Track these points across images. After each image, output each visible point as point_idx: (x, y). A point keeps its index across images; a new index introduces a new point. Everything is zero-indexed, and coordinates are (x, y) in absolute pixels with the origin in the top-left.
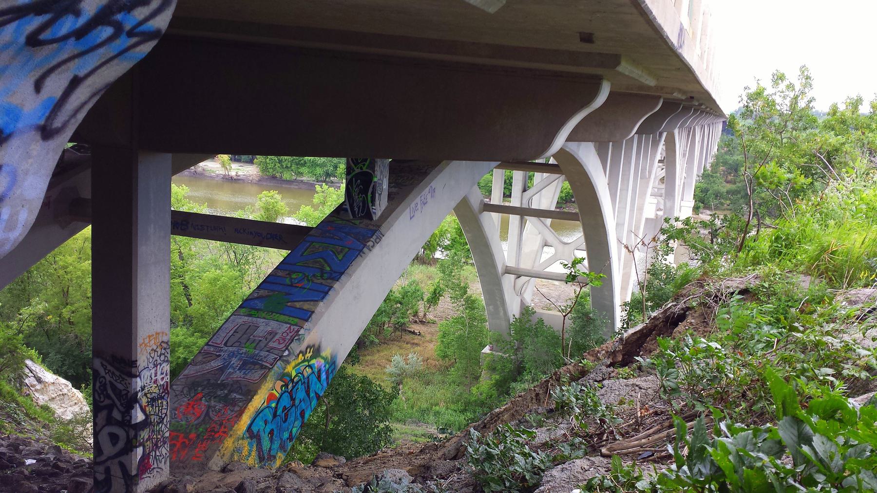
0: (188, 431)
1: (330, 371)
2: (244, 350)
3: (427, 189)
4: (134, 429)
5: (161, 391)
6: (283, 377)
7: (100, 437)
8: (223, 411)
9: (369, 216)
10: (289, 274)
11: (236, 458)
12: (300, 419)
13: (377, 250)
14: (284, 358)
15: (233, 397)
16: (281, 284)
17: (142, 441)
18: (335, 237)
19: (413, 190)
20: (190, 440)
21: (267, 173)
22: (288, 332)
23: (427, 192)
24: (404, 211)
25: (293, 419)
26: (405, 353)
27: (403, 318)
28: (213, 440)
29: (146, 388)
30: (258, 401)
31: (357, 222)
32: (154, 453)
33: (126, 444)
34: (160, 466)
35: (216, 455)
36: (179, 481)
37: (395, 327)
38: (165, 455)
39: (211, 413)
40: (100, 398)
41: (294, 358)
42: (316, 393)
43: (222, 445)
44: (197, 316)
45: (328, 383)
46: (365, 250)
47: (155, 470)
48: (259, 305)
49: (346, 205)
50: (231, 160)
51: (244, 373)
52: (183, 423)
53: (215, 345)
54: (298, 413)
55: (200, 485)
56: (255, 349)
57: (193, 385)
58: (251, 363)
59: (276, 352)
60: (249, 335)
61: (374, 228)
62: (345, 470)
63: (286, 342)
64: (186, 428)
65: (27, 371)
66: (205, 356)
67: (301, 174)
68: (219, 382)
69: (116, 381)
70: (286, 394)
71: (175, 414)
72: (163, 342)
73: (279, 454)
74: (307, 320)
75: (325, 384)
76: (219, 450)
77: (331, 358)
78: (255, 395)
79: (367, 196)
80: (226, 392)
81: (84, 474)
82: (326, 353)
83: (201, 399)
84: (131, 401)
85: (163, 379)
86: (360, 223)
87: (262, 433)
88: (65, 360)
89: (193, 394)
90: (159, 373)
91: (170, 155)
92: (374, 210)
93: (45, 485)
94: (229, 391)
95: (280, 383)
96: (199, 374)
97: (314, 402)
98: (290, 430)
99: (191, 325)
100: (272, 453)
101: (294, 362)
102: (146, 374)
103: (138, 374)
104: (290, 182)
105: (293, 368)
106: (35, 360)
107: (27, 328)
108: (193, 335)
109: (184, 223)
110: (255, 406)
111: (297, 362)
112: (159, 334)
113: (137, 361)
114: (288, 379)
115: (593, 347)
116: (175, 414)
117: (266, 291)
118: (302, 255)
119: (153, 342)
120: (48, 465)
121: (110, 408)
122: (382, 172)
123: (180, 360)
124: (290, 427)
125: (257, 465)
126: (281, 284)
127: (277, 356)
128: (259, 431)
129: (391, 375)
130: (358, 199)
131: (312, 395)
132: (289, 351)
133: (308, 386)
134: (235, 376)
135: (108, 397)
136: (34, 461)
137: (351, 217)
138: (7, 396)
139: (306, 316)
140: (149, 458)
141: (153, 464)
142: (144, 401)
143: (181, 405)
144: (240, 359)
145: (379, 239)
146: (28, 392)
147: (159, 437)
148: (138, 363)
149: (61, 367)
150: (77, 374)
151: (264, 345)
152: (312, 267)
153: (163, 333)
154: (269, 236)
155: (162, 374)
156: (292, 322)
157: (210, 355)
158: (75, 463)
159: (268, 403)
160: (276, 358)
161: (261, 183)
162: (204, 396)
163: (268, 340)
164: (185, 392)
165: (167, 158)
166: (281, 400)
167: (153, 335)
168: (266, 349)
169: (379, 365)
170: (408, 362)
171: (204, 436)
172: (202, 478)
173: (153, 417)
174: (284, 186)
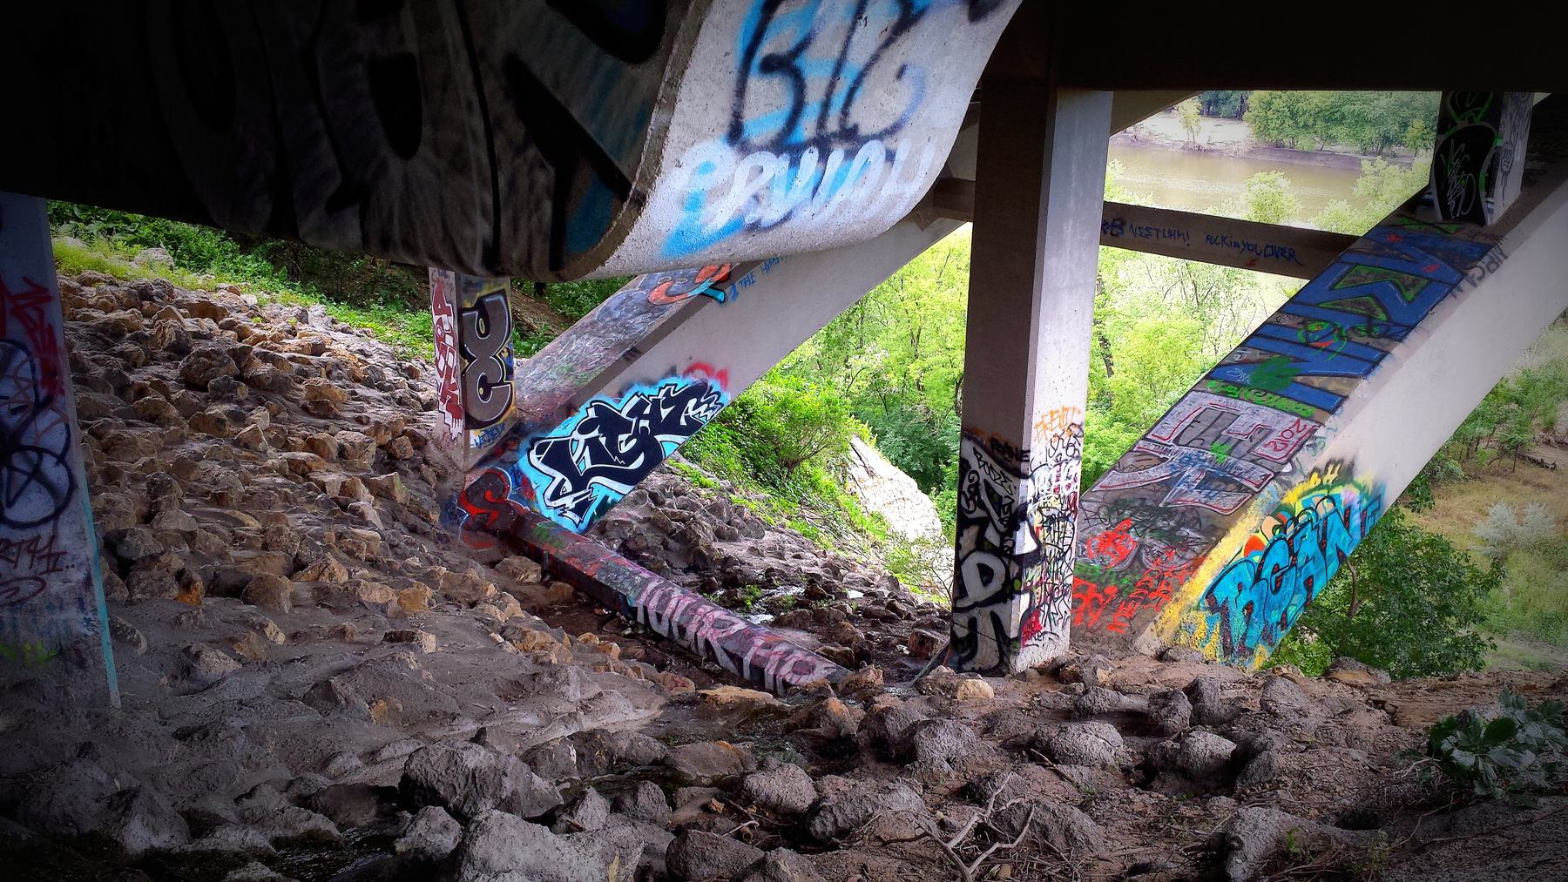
4: (1018, 564)
5: (1065, 506)
6: (1277, 510)
7: (964, 568)
8: (1165, 556)
9: (1477, 216)
11: (1183, 639)
12: (1305, 592)
15: (1185, 534)
17: (1029, 584)
18: (1404, 256)
20: (1106, 596)
21: (1267, 139)
22: (1293, 429)
25: (1290, 589)
27: (1520, 432)
28: (1145, 602)
29: (1041, 498)
30: (1229, 548)
31: (1452, 228)
32: (1047, 607)
33: (1004, 585)
35: (1148, 630)
36: (1086, 661)
37: (1502, 449)
39: (1144, 556)
40: (969, 506)
41: (1302, 478)
42: (1339, 551)
44: (1121, 393)
45: (1363, 534)
46: (1464, 284)
47: (1047, 636)
49: (1430, 193)
51: (1206, 496)
52: (1096, 565)
53: (1159, 441)
54: (1302, 580)
55: (1120, 674)
57: (1116, 505)
59: (1269, 464)
60: (1220, 429)
62: (1391, 696)
63: (1288, 449)
64: (1100, 576)
66: (1138, 458)
67: (1332, 139)
68: (1161, 505)
70: (1282, 543)
71: (1084, 550)
74: (1332, 412)
75: (1357, 536)
76: (1155, 622)
77: (1374, 487)
78: (1224, 535)
80: (1172, 523)
81: (933, 626)
82: (1365, 476)
83: (1128, 530)
84: (1017, 517)
87: (1231, 606)
88: (908, 446)
89: (1115, 521)
91: (1111, 94)
92: (1490, 206)
93: (874, 633)
94: (1177, 523)
95: (1272, 522)
96: (1127, 486)
97: (1333, 566)
99: (1108, 408)
100: (1248, 643)
101: (1301, 486)
102: (1042, 474)
103: (1030, 473)
104: (1307, 155)
105: (1299, 498)
106: (867, 440)
107: (857, 390)
108: (1112, 425)
110: (1222, 555)
113: (1029, 451)
114: (1288, 516)
116: (1084, 550)
117: (1258, 352)
118: (1331, 289)
119: (1056, 423)
120: (880, 603)
121: (983, 523)
122: (1514, 128)
123: (1090, 465)
124: (1285, 604)
125: (1218, 660)
128: (1226, 601)
130: (1458, 184)
131: (1330, 551)
132: (1293, 464)
133: (1324, 535)
134: (1189, 497)
135: (981, 505)
136: (861, 595)
137: (1440, 217)
138: (824, 491)
139: (1332, 403)
142: (1036, 520)
144: (1201, 470)
146: (854, 489)
147: (1056, 582)
148: (1032, 455)
149: (903, 457)
150: (925, 470)
151: (1247, 449)
152: (1351, 312)
153: (1074, 409)
154: (1269, 251)
156: (1303, 414)
157: (1147, 457)
158: (919, 607)
159: (1246, 553)
161: (1253, 156)
162: (1133, 526)
163: (1254, 442)
164: (1102, 515)
165: (1104, 101)
166: (1271, 552)
168: (1249, 457)
169: (1459, 518)
170: (1524, 520)
171: (1130, 594)
172: (1122, 664)
173: (1048, 548)
174: (1296, 162)
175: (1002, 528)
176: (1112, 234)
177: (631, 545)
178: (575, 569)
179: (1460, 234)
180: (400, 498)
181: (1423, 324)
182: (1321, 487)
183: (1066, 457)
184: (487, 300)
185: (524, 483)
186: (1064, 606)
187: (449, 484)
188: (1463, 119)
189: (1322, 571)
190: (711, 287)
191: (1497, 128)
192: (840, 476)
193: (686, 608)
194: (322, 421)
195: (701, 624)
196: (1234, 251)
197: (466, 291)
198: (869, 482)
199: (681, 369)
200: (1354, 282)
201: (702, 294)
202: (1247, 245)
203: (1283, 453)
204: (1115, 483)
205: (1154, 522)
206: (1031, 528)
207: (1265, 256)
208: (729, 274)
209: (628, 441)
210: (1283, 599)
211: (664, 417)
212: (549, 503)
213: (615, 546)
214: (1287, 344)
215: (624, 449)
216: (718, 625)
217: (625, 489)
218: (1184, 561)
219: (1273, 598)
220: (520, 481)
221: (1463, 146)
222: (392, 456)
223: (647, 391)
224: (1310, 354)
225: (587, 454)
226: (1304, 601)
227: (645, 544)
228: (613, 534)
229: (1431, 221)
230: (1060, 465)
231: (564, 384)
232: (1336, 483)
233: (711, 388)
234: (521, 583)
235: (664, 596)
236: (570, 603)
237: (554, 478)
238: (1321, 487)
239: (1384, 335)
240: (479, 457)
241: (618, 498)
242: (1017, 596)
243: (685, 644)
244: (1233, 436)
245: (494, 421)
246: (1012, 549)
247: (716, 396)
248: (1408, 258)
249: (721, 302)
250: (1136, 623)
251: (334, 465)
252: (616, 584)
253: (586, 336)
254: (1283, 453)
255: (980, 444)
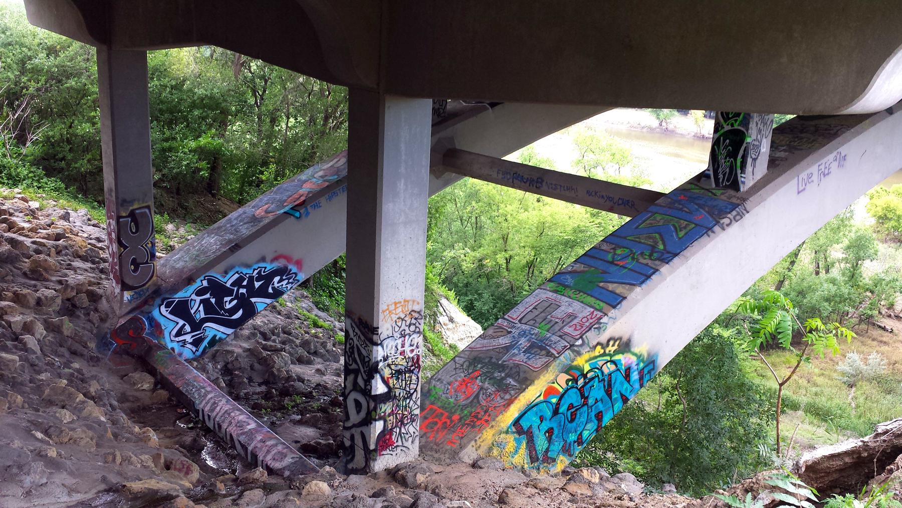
0: (453, 411)
1: (646, 371)
2: (536, 331)
3: (831, 157)
4: (373, 401)
5: (410, 364)
9: (735, 185)
10: (614, 249)
11: (495, 452)
12: (596, 422)
13: (735, 229)
14: (576, 348)
15: (508, 382)
16: (602, 260)
19: (808, 156)
20: (452, 421)
23: (831, 160)
24: (788, 182)
26: (867, 350)
28: (473, 427)
29: (390, 358)
30: (533, 393)
31: (719, 192)
32: (398, 430)
34: (406, 444)
35: (470, 446)
38: (413, 434)
39: (481, 395)
41: (588, 349)
42: (622, 395)
43: (481, 435)
46: (717, 228)
47: (399, 449)
48: (570, 280)
50: (705, 116)
51: (528, 357)
52: (452, 400)
54: (593, 414)
56: (548, 331)
58: (539, 347)
59: (569, 339)
60: (547, 314)
61: (738, 202)
63: (582, 329)
65: (441, 310)
68: (500, 362)
69: (361, 345)
70: (574, 390)
71: (448, 389)
72: (413, 311)
73: (561, 457)
74: (614, 307)
76: (476, 441)
77: (649, 355)
78: (530, 385)
79: (736, 160)
83: (476, 378)
84: (373, 370)
85: (412, 351)
86: (722, 194)
88: (497, 303)
90: (407, 344)
92: (743, 179)
98: (579, 433)
100: (550, 454)
101: (587, 354)
109: (540, 180)
110: (527, 398)
111: (592, 354)
112: (408, 301)
113: (378, 328)
114: (578, 373)
115: (731, 480)
116: (448, 389)
117: (583, 266)
118: (637, 228)
119: (400, 309)
121: (356, 372)
122: (760, 131)
126: (602, 260)
127: (567, 344)
128: (531, 427)
129: (843, 374)
131: (615, 395)
132: (583, 340)
135: (355, 361)
137: (714, 186)
139: (615, 301)
140: (391, 435)
141: (397, 441)
142: (387, 373)
143: (456, 381)
144: (529, 341)
145: (741, 216)
146: (440, 330)
147: (406, 413)
154: (620, 202)
155: (411, 345)
156: (598, 307)
160: (565, 346)
162: (480, 375)
166: (566, 396)
167: (401, 302)
169: (831, 360)
175: (365, 377)
176: (536, 187)
177: (230, 366)
178: (171, 383)
179: (724, 195)
180: (66, 332)
181: (685, 253)
182: (604, 354)
183: (409, 332)
184: (137, 211)
185: (157, 328)
186: (413, 429)
187: (107, 325)
188: (728, 125)
189: (609, 408)
190: (292, 209)
191: (747, 130)
192: (432, 322)
193: (225, 412)
194: (33, 282)
195: (230, 423)
196: (602, 201)
197: (122, 205)
198: (451, 325)
199: (268, 258)
200: (651, 224)
201: (285, 213)
202: (609, 198)
203: (578, 332)
204: (478, 346)
205: (493, 373)
206: (383, 379)
207: (618, 205)
208: (304, 201)
209: (231, 301)
210: (578, 426)
211: (257, 287)
212: (173, 339)
213: (219, 367)
214: (601, 262)
215: (228, 306)
216: (240, 425)
217: (229, 331)
218: (503, 400)
219: (570, 425)
220: (153, 324)
221: (728, 141)
222: (74, 306)
223: (245, 271)
224: (613, 269)
225: (201, 308)
226: (595, 427)
227: (239, 366)
228: (219, 359)
229: (708, 187)
230: (405, 337)
231: (190, 265)
232: (616, 352)
233: (291, 270)
234: (138, 390)
235: (215, 403)
236: (165, 404)
237: (178, 323)
238: (604, 354)
239: (658, 259)
240: (130, 308)
241: (224, 336)
242: (374, 422)
243: (221, 435)
244: (553, 319)
245: (144, 285)
246: (370, 391)
247: (294, 275)
248: (687, 211)
249: (297, 218)
250: (465, 440)
251: (29, 311)
252: (191, 393)
253: (213, 236)
254: (578, 332)
255: (353, 320)
